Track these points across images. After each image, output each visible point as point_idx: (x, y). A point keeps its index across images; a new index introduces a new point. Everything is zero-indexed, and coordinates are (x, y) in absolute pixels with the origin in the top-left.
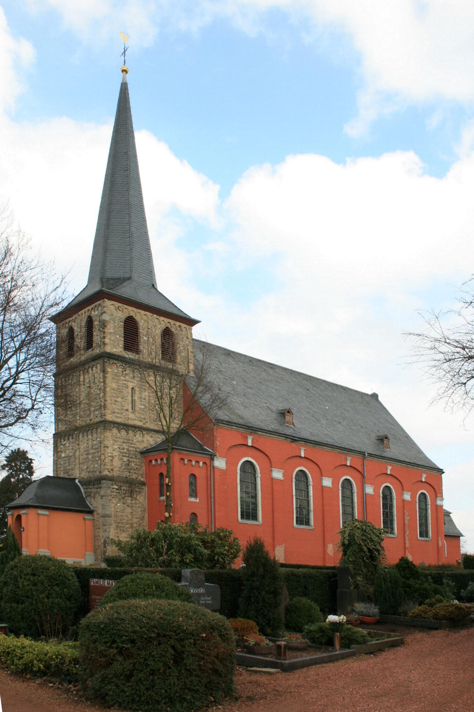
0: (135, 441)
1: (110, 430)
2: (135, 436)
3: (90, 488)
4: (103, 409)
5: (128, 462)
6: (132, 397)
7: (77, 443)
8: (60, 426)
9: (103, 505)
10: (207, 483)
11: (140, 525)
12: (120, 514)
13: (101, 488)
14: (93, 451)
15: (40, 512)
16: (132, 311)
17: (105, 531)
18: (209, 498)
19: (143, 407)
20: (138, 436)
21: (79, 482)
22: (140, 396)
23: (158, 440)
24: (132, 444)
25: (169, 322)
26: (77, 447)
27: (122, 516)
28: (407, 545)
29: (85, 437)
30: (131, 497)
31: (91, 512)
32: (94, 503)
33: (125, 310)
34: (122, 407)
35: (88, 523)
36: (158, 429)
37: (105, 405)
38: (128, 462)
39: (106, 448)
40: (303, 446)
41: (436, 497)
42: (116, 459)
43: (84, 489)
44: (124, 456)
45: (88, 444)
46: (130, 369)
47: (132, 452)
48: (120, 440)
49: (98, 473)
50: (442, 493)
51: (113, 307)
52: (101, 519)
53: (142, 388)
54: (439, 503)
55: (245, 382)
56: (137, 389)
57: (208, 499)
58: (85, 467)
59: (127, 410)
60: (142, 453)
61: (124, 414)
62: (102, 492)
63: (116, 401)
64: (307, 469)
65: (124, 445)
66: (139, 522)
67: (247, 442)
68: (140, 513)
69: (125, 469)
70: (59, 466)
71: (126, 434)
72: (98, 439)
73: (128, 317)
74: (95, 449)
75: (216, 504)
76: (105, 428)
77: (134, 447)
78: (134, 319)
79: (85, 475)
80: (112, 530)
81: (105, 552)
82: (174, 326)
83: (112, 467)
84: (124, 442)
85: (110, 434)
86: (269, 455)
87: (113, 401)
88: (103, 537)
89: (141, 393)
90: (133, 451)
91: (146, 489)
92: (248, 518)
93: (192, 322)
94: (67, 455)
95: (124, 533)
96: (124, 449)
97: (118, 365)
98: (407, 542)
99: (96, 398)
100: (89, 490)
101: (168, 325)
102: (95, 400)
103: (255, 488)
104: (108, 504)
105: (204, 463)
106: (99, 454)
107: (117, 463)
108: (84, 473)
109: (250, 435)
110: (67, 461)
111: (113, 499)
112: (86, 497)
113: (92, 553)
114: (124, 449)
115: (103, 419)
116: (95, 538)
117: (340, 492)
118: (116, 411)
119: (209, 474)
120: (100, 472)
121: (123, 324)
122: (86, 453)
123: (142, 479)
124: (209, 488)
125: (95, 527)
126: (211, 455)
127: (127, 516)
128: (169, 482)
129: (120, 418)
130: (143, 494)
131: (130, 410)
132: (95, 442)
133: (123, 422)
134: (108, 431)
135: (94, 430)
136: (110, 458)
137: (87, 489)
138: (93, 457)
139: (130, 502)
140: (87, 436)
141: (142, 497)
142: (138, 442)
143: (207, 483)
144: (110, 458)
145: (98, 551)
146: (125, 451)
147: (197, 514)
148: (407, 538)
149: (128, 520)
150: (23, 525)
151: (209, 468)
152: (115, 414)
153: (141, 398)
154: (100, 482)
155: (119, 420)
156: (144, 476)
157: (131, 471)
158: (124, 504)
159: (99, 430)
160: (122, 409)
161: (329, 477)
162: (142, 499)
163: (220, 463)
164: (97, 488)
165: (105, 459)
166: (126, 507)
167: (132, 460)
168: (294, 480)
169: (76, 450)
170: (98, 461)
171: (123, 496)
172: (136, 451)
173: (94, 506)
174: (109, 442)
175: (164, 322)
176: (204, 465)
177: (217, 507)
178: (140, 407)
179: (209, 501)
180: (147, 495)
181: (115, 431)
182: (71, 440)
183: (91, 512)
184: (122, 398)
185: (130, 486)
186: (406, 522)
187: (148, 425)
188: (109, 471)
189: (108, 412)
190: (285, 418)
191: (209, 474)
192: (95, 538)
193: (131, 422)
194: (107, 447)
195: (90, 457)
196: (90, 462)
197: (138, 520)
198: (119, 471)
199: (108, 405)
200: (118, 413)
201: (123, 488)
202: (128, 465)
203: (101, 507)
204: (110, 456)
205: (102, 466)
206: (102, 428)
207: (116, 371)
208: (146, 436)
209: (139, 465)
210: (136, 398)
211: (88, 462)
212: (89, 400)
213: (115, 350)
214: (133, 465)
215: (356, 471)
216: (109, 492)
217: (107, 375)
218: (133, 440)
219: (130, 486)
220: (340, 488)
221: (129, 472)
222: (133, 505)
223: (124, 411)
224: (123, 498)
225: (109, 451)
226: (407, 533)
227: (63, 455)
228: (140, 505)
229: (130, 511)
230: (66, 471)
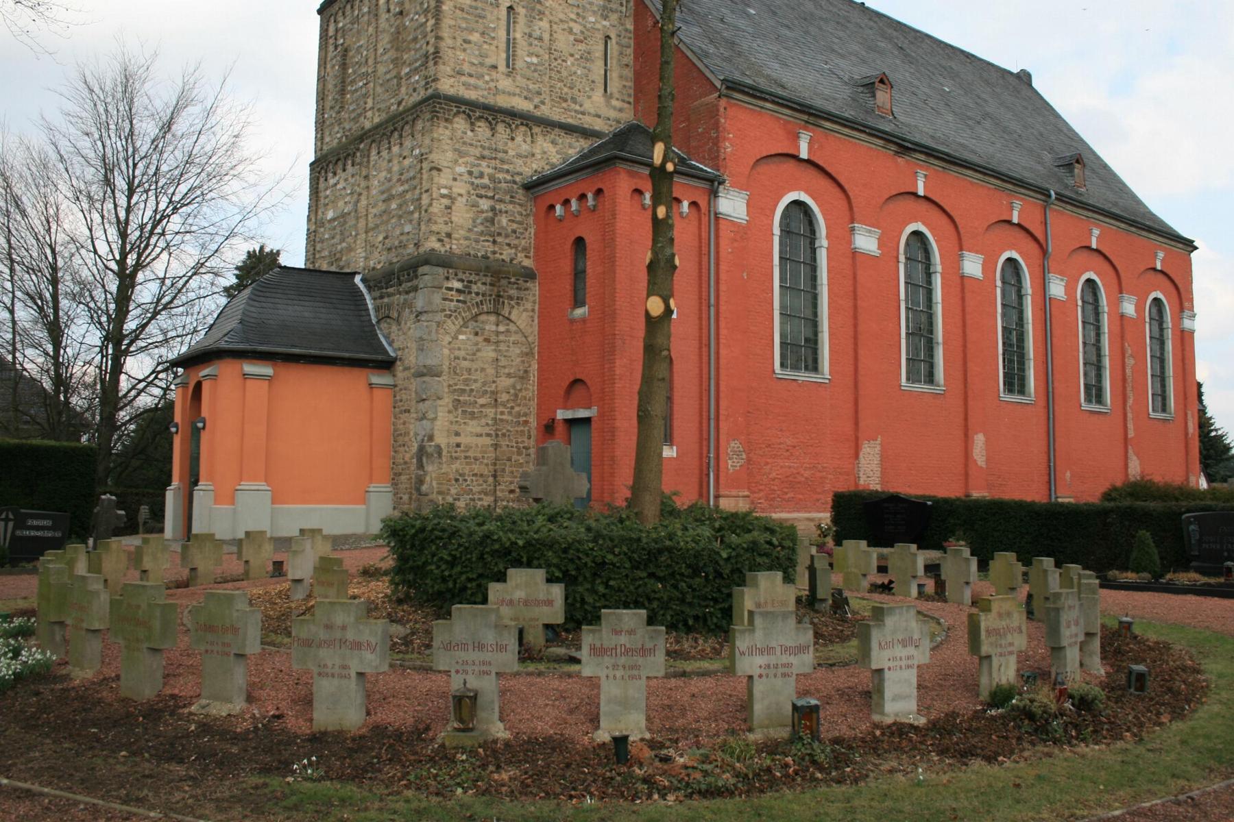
0: (511, 153)
1: (447, 120)
2: (513, 139)
3: (389, 295)
4: (431, 63)
5: (490, 214)
6: (508, 34)
7: (364, 173)
8: (327, 139)
9: (421, 339)
10: (700, 264)
11: (516, 395)
12: (465, 364)
13: (416, 289)
14: (401, 189)
15: (250, 368)
17: (424, 417)
18: (704, 308)
19: (535, 60)
20: (519, 139)
21: (363, 280)
22: (527, 31)
23: (571, 151)
24: (502, 161)
26: (363, 184)
27: (469, 371)
28: (1131, 434)
29: (384, 153)
30: (498, 314)
31: (387, 365)
32: (398, 339)
34: (480, 59)
35: (378, 393)
37: (437, 52)
38: (490, 214)
39: (434, 173)
40: (921, 168)
41: (1182, 309)
42: (461, 202)
43: (374, 299)
44: (481, 196)
45: (389, 171)
47: (503, 185)
48: (472, 151)
49: (411, 249)
50: (1192, 300)
52: (414, 384)
53: (533, 9)
54: (1187, 324)
55: (775, 13)
56: (521, 11)
57: (700, 310)
58: (381, 238)
59: (495, 67)
60: (529, 187)
61: (487, 78)
62: (420, 302)
63: (465, 41)
64: (931, 230)
65: (484, 164)
66: (514, 387)
67: (798, 148)
68: (519, 359)
69: (482, 233)
70: (318, 247)
71: (488, 133)
72: (417, 152)
74: (407, 181)
75: (722, 324)
76: (435, 116)
77: (508, 171)
79: (378, 261)
80: (440, 414)
81: (421, 481)
83: (447, 229)
84: (483, 157)
85: (448, 132)
86: (846, 187)
87: (459, 41)
88: (416, 434)
89: (530, 20)
91: (535, 288)
94: (339, 212)
95: (474, 422)
96: (481, 176)
98: (1130, 426)
99: (415, 40)
100: (386, 300)
102: (412, 46)
103: (814, 278)
104: (434, 336)
105: (694, 204)
106: (417, 192)
107: (462, 215)
108: (376, 254)
109: (806, 129)
110: (338, 230)
111: (449, 321)
112: (379, 322)
113: (386, 487)
114: (481, 176)
115: (430, 91)
116: (398, 438)
117: (999, 291)
118: (466, 68)
119: (704, 235)
120: (417, 245)
122: (385, 196)
123: (527, 263)
124: (704, 278)
125: (399, 409)
126: (711, 181)
127: (483, 370)
128: (665, 159)
129: (476, 88)
130: (529, 306)
131: (502, 67)
132: (407, 162)
133: (482, 100)
134: (443, 124)
135: (407, 127)
136: (446, 201)
137: (382, 297)
138: (400, 206)
139: (494, 328)
140: (389, 148)
141: (525, 314)
142: (519, 156)
143: (700, 264)
144: (446, 201)
145: (403, 478)
146: (486, 181)
148: (1130, 415)
149: (484, 384)
150: (205, 412)
151: (705, 219)
152: (463, 79)
153: (530, 36)
154: (415, 272)
155: (472, 95)
156: (532, 254)
157: (499, 239)
158: (477, 334)
159: (419, 125)
160: (481, 64)
161: (977, 252)
162: (525, 316)
163: (732, 205)
164: (407, 293)
165: (431, 205)
166: (482, 344)
167: (502, 207)
168: (902, 258)
169: (360, 194)
170: (412, 213)
171: (475, 311)
172: (515, 182)
173: (396, 345)
174: (444, 156)
177: (723, 332)
178: (528, 59)
179: (704, 316)
180: (537, 308)
181: (460, 123)
182: (349, 167)
183: (387, 365)
184: (483, 34)
185: (494, 281)
186: (1128, 371)
187: (546, 111)
188: (440, 240)
189: (445, 69)
190: (874, 96)
191: (704, 235)
192: (398, 438)
193: (503, 102)
194: (439, 170)
195: (394, 206)
196: (393, 221)
197: (512, 380)
198: (467, 239)
199: (447, 54)
200: (471, 75)
201: (474, 288)
202: (492, 221)
203: (413, 346)
204: (443, 196)
205: (423, 227)
206: (428, 116)
208: (540, 139)
209: (520, 223)
210: (518, 35)
211: (387, 222)
212: (397, 49)
214: (504, 221)
215: (1029, 239)
216: (437, 298)
218: (506, 152)
219: (494, 281)
220: (999, 283)
221: (494, 242)
222: (501, 338)
223: (485, 71)
224: (475, 318)
225: (443, 181)
226: (1130, 402)
227: (330, 215)
228: (518, 337)
229: (493, 355)
230: (335, 257)
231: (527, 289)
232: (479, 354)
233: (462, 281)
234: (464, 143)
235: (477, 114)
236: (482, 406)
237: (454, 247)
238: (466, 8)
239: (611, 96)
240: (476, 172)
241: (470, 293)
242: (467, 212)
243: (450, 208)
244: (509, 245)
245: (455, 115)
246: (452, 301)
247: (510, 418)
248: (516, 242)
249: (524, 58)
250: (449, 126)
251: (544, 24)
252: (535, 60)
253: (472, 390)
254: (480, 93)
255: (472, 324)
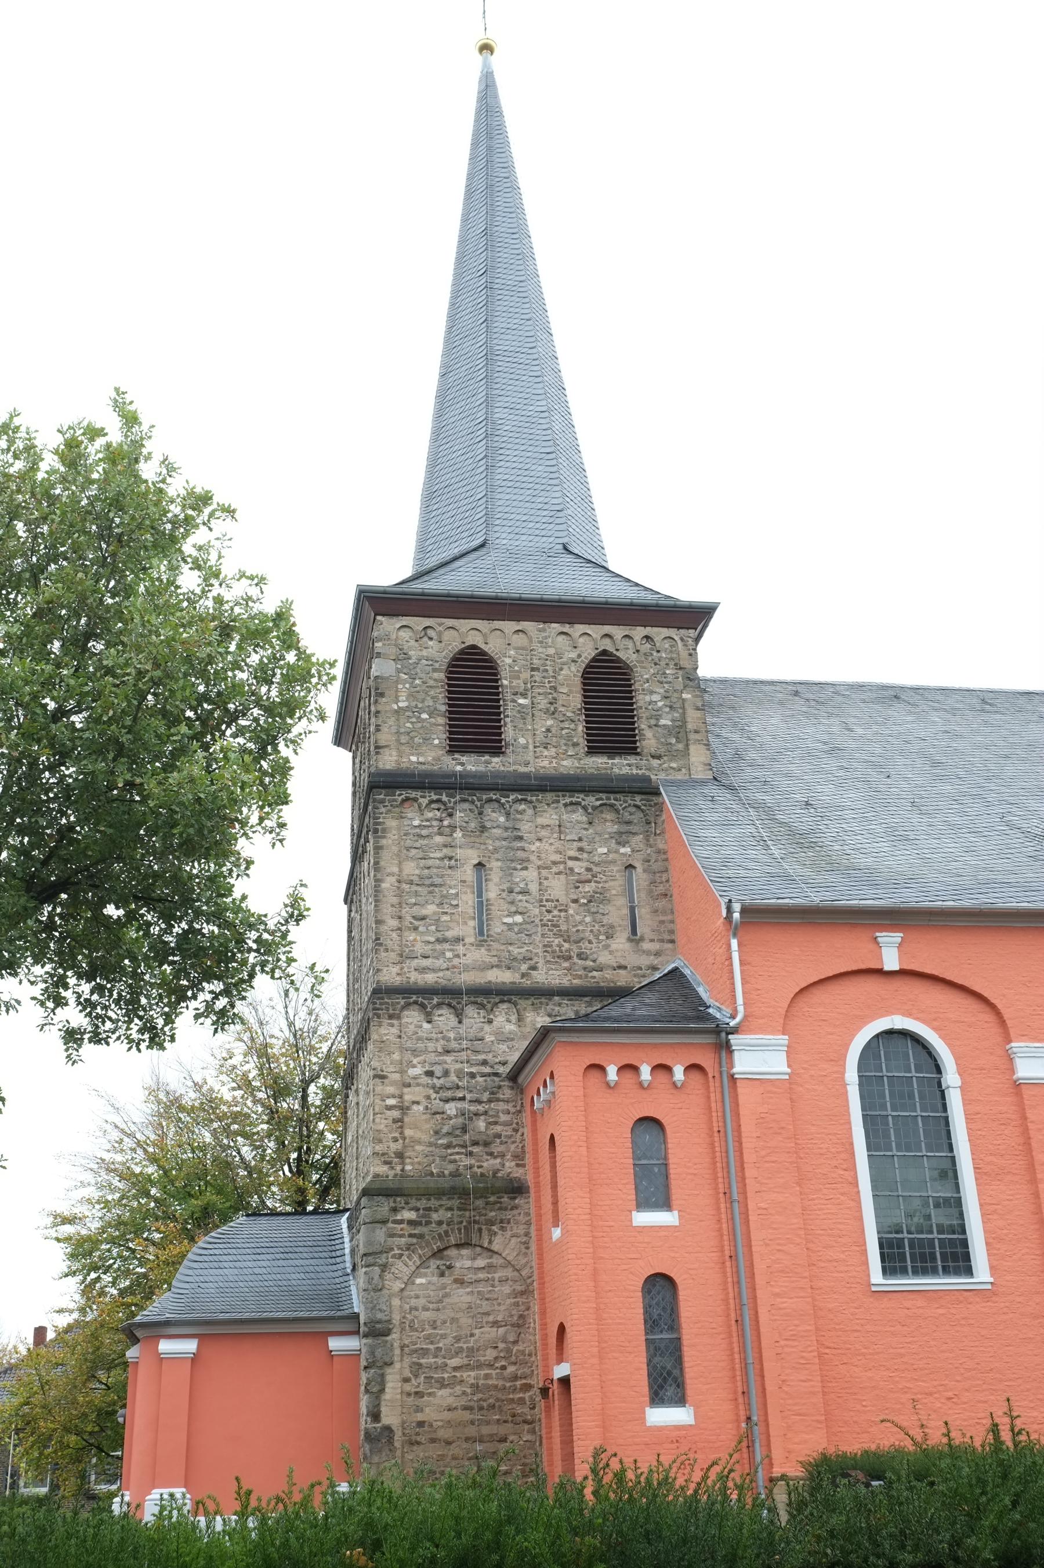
0: (489, 1038)
1: (391, 1017)
2: (490, 1022)
12: (426, 1315)
16: (470, 632)
25: (607, 635)
33: (448, 635)
36: (576, 982)
44: (447, 1101)
46: (466, 806)
48: (431, 1046)
51: (405, 634)
65: (448, 1059)
71: (453, 1020)
73: (462, 652)
78: (483, 653)
82: (626, 643)
85: (395, 1031)
89: (508, 873)
90: (483, 1075)
92: (925, 1265)
93: (695, 617)
97: (424, 802)
101: (607, 645)
105: (693, 1068)
121: (442, 676)
127: (454, 1320)
133: (443, 982)
136: (396, 1114)
141: (514, 1240)
144: (396, 1114)
147: (678, 1281)
149: (458, 1339)
175: (586, 641)
176: (696, 1076)
178: (509, 920)
204: (390, 1108)
207: (416, 823)
213: (414, 759)
217: (384, 842)
228: (509, 1273)
231: (515, 1207)
232: (447, 1300)
233: (417, 1210)
234: (419, 1039)
235: (435, 1001)
236: (455, 1369)
237: (408, 1168)
238: (416, 879)
239: (642, 939)
240: (438, 1070)
241: (428, 1223)
242: (427, 1121)
243: (401, 1120)
244: (491, 1154)
245: (403, 1008)
246: (401, 1236)
247: (500, 1383)
248: (502, 1148)
249: (502, 920)
250: (395, 1022)
251: (531, 874)
252: (519, 919)
253: (439, 1349)
254: (441, 974)
255: (434, 1263)
